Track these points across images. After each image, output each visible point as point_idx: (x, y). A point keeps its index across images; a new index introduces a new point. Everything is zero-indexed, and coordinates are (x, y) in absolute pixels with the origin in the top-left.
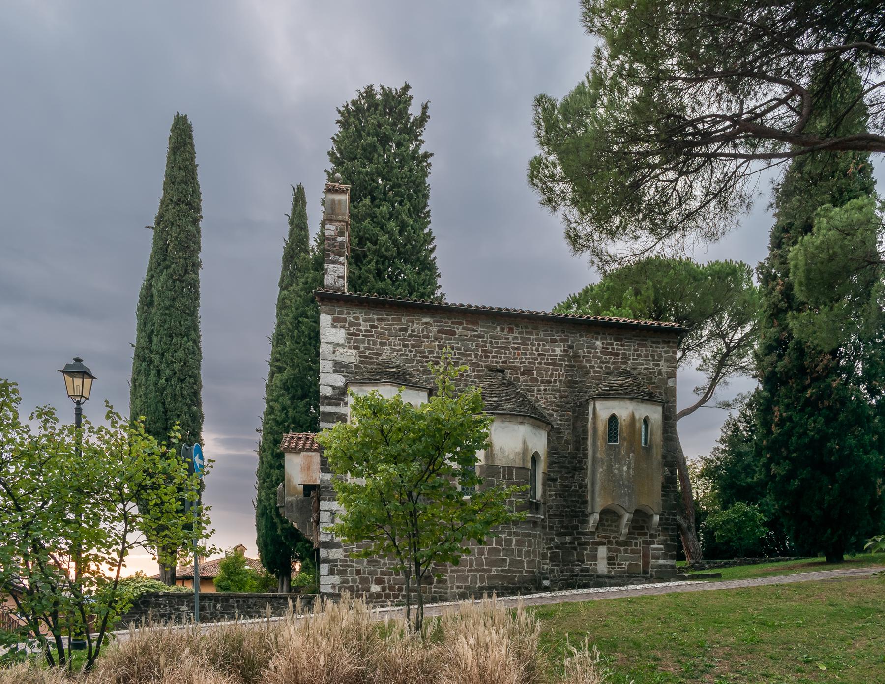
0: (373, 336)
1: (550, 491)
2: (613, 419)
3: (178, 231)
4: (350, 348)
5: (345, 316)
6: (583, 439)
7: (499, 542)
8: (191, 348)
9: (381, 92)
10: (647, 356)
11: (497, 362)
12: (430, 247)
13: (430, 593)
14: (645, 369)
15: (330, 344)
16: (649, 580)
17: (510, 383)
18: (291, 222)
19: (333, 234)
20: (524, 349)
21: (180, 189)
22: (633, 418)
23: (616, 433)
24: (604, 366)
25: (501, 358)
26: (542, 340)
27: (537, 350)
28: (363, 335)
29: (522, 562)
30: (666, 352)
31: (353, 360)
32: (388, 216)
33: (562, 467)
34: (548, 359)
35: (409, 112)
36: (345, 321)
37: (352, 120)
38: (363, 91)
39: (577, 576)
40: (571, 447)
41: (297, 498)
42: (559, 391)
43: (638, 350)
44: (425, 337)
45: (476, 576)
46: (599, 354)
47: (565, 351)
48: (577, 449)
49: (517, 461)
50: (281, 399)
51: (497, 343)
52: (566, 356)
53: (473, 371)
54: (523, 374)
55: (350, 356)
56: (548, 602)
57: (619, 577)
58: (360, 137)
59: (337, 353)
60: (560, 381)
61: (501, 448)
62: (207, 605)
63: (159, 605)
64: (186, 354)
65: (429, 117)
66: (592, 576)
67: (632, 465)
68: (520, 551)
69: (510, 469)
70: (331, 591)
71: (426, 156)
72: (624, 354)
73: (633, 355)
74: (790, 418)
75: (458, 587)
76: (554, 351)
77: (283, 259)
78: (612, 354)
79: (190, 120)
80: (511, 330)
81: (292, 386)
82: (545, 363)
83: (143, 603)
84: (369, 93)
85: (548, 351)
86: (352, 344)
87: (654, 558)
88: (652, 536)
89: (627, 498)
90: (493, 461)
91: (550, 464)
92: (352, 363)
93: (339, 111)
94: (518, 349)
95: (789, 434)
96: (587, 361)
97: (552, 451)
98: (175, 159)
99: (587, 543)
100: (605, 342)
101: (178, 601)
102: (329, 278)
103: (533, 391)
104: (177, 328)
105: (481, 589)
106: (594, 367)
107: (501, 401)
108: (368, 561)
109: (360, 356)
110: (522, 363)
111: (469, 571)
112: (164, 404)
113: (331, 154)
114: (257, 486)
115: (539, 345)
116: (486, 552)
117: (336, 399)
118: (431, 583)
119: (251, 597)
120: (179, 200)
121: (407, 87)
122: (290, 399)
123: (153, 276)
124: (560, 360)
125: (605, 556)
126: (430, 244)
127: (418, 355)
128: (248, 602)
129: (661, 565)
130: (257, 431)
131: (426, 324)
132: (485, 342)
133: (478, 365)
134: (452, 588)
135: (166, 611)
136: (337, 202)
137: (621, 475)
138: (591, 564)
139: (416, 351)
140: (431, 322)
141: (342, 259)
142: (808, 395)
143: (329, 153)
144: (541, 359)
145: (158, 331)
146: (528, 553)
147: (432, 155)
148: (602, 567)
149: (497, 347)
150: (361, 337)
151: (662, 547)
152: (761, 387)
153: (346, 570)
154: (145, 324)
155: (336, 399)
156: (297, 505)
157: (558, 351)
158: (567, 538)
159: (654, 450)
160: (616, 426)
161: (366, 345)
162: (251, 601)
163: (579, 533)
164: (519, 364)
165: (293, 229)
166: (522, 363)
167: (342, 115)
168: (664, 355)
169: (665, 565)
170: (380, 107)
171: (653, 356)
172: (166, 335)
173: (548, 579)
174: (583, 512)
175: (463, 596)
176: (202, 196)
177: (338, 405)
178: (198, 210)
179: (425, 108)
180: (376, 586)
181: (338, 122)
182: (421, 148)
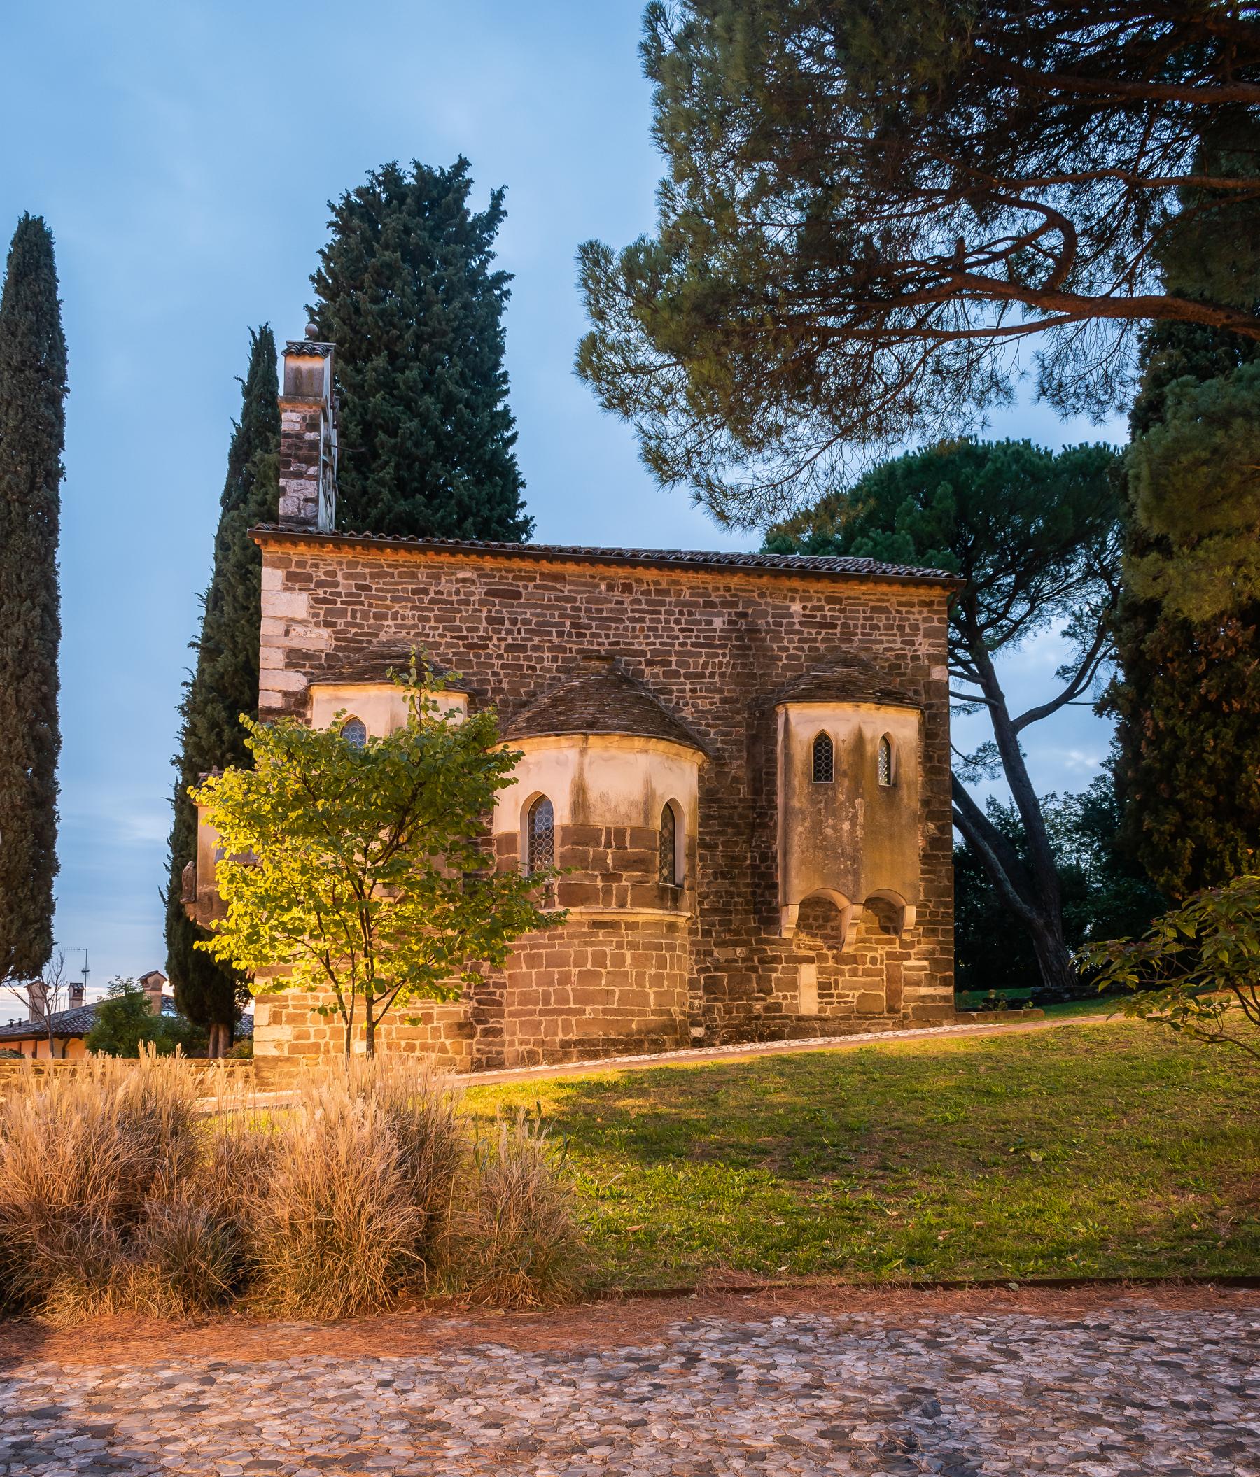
0: (362, 603)
1: (704, 867)
2: (822, 743)
4: (317, 625)
6: (767, 774)
8: (38, 620)
9: (415, 172)
10: (889, 627)
11: (599, 644)
12: (507, 434)
14: (886, 650)
16: (902, 1024)
17: (624, 679)
18: (247, 392)
19: (297, 427)
20: (652, 620)
21: (26, 345)
22: (860, 740)
23: (829, 764)
24: (806, 646)
25: (607, 636)
26: (686, 604)
27: (677, 622)
29: (646, 995)
30: (925, 620)
31: (322, 646)
32: (421, 386)
33: (728, 825)
34: (697, 637)
35: (466, 205)
37: (356, 222)
38: (379, 171)
39: (757, 1018)
40: (744, 790)
42: (721, 691)
43: (872, 619)
44: (460, 602)
46: (797, 627)
47: (730, 622)
48: (756, 791)
49: (634, 816)
50: (209, 707)
51: (600, 611)
52: (732, 631)
53: (555, 659)
54: (649, 663)
55: (320, 639)
56: (637, 1068)
57: (842, 1018)
58: (371, 253)
59: (293, 633)
60: (723, 675)
61: (602, 795)
64: (28, 631)
65: (505, 213)
66: (788, 1017)
67: (861, 820)
68: (641, 976)
69: (620, 833)
70: (276, 1053)
71: (502, 277)
72: (845, 625)
73: (864, 626)
74: (1172, 731)
76: (710, 623)
77: (231, 456)
78: (822, 626)
79: (49, 224)
81: (232, 685)
82: (693, 645)
84: (391, 176)
85: (699, 622)
87: (908, 984)
88: (904, 944)
89: (850, 878)
90: (586, 817)
91: (705, 820)
93: (333, 207)
94: (642, 620)
95: (1170, 760)
96: (773, 640)
97: (708, 796)
98: (18, 294)
99: (776, 959)
100: (809, 605)
102: (289, 502)
103: (670, 692)
105: (565, 1044)
106: (787, 649)
107: (603, 712)
111: (542, 1013)
113: (318, 279)
114: (169, 865)
115: (681, 613)
116: (574, 979)
120: (23, 363)
121: (463, 164)
122: (225, 708)
124: (721, 638)
125: (814, 982)
126: (507, 429)
129: (923, 998)
131: (464, 580)
132: (578, 609)
133: (564, 650)
134: (512, 1043)
137: (839, 838)
138: (785, 997)
139: (445, 629)
141: (312, 470)
142: (1202, 691)
143: (312, 278)
144: (686, 637)
146: (657, 980)
147: (511, 277)
148: (808, 1002)
149: (600, 619)
151: (925, 963)
152: (1121, 678)
153: (303, 1015)
157: (718, 623)
158: (739, 950)
159: (904, 792)
160: (829, 751)
163: (760, 942)
164: (643, 647)
167: (339, 213)
168: (922, 625)
169: (933, 998)
170: (409, 200)
171: (901, 628)
173: (699, 1025)
174: (770, 903)
176: (69, 356)
178: (62, 378)
179: (497, 197)
181: (331, 224)
182: (489, 265)
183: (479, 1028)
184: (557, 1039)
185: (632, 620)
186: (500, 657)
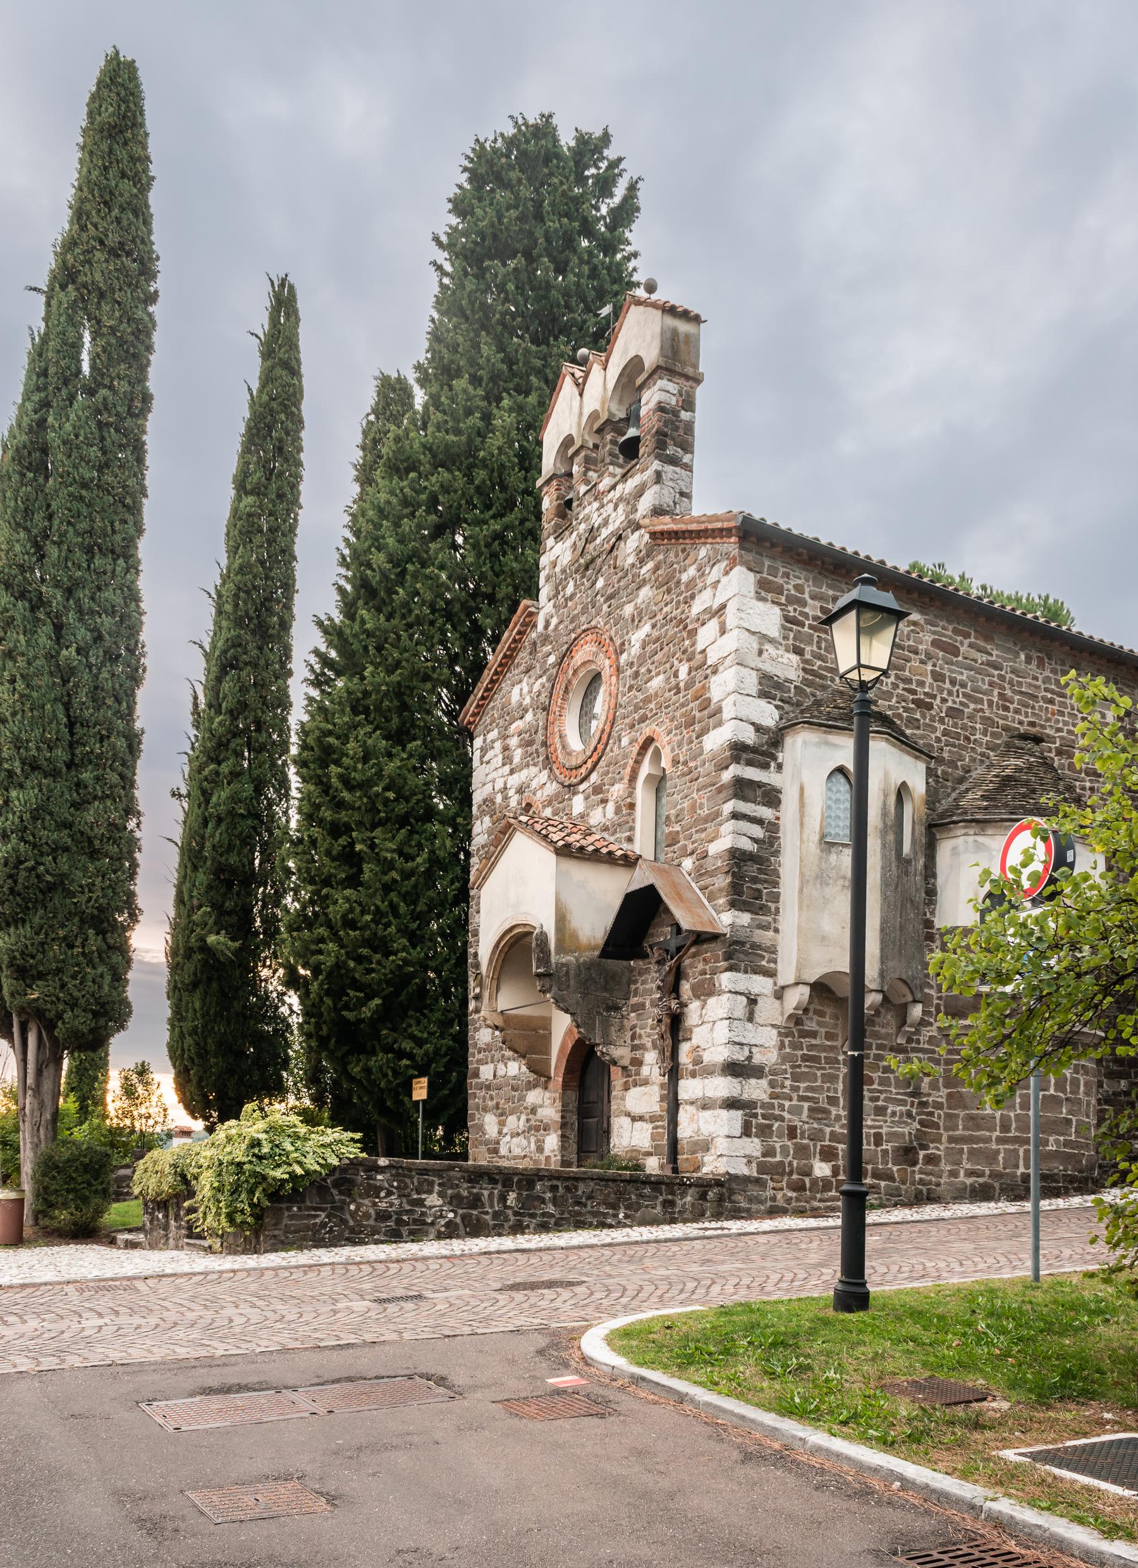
3: (117, 314)
4: (787, 651)
5: (780, 580)
7: (1060, 1086)
11: (1021, 723)
13: (913, 1183)
15: (754, 633)
19: (674, 402)
21: (125, 223)
28: (811, 627)
36: (779, 590)
41: (577, 959)
45: (1016, 1151)
51: (1020, 684)
59: (765, 655)
62: (486, 1193)
63: (377, 1190)
75: (970, 1173)
80: (1041, 664)
83: (336, 1184)
86: (791, 642)
92: (791, 682)
94: (1051, 701)
101: (420, 1183)
104: (105, 535)
108: (810, 1109)
109: (804, 670)
110: (1059, 730)
111: (1000, 1140)
112: (67, 706)
117: (763, 754)
118: (914, 1163)
119: (583, 1179)
120: (121, 244)
123: (45, 404)
127: (901, 685)
128: (576, 1189)
130: (174, 795)
134: (954, 1174)
135: (392, 1205)
136: (681, 338)
140: (922, 622)
145: (63, 535)
150: (806, 629)
154: (28, 512)
155: (763, 754)
156: (578, 975)
158: (1123, 1082)
161: (815, 648)
162: (582, 1188)
165: (273, 368)
166: (1059, 730)
172: (81, 546)
175: (982, 1194)
177: (765, 766)
180: (823, 1165)
183: (922, 1153)
184: (1019, 1172)
185: (1045, 699)
186: (942, 720)
